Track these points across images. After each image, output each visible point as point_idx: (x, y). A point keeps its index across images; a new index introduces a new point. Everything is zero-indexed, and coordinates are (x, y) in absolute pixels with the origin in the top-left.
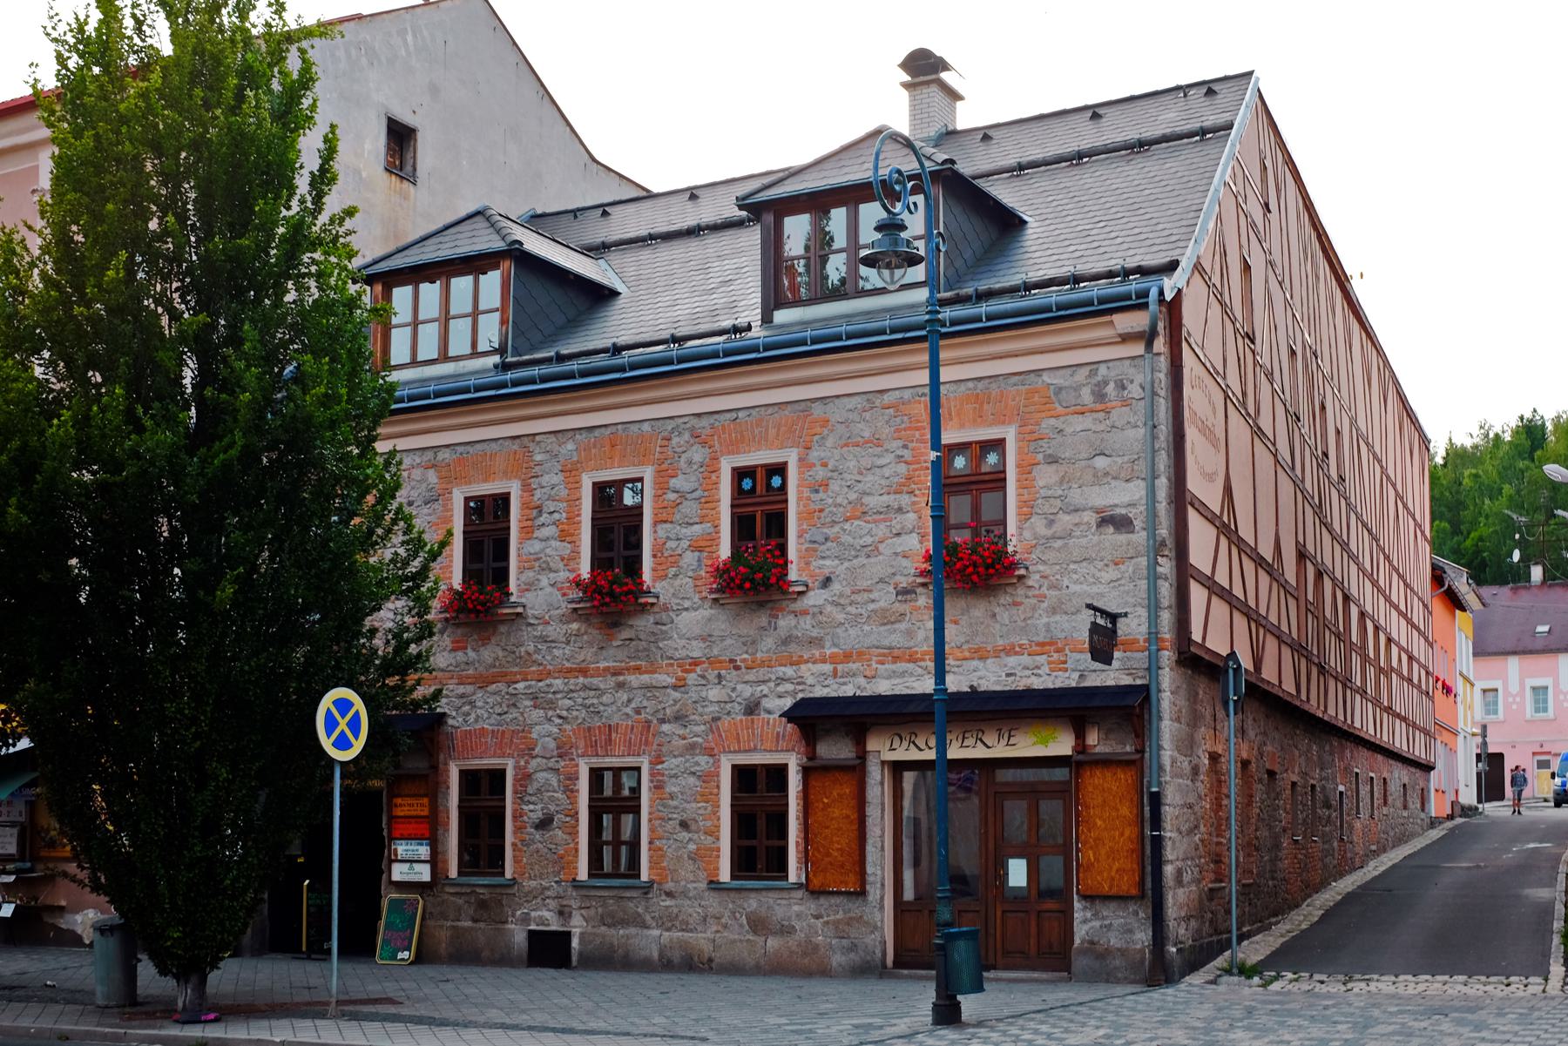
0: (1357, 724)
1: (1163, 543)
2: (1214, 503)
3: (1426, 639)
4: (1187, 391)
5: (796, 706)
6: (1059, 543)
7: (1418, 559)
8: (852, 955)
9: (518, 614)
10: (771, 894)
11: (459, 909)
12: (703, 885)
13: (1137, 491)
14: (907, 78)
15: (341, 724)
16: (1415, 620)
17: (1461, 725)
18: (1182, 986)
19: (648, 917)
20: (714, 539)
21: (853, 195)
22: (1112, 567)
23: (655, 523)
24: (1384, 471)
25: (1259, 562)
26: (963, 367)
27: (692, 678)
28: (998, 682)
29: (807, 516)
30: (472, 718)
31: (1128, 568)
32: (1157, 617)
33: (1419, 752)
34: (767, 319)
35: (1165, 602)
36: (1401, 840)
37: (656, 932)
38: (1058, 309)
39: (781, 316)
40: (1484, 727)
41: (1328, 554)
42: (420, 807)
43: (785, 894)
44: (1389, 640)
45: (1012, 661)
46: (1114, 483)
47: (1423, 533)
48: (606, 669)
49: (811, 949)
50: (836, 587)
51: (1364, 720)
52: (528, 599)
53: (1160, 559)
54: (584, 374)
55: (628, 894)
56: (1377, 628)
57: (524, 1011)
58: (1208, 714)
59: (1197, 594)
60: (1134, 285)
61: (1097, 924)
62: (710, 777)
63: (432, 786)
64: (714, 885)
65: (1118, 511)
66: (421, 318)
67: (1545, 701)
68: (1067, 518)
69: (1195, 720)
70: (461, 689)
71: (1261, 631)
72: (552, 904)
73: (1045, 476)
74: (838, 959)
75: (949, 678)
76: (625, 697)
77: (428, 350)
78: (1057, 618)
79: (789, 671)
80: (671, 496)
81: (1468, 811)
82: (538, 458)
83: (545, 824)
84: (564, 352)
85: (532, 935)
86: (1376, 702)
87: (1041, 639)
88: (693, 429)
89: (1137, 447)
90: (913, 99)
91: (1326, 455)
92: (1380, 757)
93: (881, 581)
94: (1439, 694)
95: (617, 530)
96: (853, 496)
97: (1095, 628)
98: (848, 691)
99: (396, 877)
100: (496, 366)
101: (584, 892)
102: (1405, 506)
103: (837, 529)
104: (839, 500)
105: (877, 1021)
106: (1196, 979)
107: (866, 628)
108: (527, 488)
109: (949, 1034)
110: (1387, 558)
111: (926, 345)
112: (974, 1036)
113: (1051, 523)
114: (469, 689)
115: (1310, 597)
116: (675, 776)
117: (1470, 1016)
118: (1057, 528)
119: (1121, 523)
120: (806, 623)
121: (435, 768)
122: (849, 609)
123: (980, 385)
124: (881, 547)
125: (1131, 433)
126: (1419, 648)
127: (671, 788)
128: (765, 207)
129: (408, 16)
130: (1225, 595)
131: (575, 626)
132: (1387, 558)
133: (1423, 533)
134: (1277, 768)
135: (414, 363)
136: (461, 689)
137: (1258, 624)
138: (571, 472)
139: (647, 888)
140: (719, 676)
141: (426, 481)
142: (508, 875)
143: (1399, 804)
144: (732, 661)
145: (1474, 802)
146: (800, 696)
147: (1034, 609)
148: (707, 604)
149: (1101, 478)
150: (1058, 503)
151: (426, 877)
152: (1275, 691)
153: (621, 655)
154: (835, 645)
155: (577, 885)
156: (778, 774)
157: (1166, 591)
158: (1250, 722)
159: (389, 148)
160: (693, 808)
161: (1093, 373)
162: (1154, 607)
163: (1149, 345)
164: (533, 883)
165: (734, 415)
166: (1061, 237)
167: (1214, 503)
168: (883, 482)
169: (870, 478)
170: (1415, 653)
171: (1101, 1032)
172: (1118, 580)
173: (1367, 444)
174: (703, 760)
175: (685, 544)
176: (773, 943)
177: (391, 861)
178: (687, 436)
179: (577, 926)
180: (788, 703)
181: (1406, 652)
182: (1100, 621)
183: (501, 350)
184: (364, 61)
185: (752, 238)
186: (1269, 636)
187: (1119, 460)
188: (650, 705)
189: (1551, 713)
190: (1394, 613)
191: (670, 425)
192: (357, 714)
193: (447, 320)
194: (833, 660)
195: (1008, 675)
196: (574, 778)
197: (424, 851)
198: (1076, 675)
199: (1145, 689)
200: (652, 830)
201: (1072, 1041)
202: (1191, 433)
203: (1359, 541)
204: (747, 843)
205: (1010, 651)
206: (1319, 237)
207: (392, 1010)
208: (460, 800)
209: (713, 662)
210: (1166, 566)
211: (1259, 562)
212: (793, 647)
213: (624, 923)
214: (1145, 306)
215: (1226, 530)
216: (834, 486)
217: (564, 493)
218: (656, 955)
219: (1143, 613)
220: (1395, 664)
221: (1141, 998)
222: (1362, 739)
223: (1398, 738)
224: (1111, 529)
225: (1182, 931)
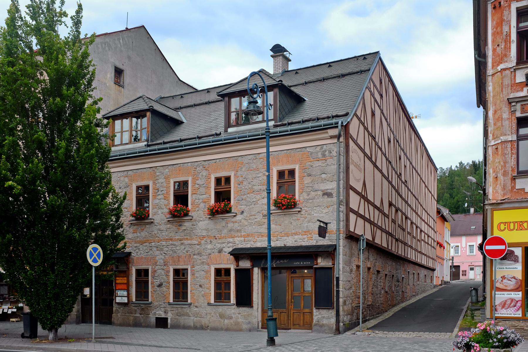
1: (342, 201)
2: (359, 189)
3: (434, 231)
4: (351, 153)
5: (233, 250)
6: (311, 201)
7: (432, 206)
8: (249, 325)
9: (152, 222)
10: (226, 307)
11: (136, 311)
12: (206, 304)
13: (334, 185)
14: (272, 53)
15: (94, 254)
16: (430, 225)
17: (445, 257)
18: (344, 335)
19: (190, 313)
20: (209, 199)
21: (241, 94)
22: (326, 208)
23: (192, 194)
24: (421, 179)
25: (375, 207)
26: (277, 147)
27: (203, 242)
28: (292, 243)
29: (236, 192)
30: (139, 253)
31: (331, 208)
32: (339, 224)
33: (430, 265)
34: (226, 131)
35: (342, 219)
36: (424, 291)
37: (192, 318)
38: (311, 128)
39: (230, 130)
40: (453, 257)
41: (400, 204)
42: (124, 280)
43: (229, 307)
44: (421, 231)
45: (296, 237)
46: (327, 182)
47: (434, 198)
48: (178, 239)
49: (237, 323)
50: (245, 214)
51: (411, 255)
52: (155, 217)
53: (341, 206)
54: (170, 148)
55: (184, 306)
56: (417, 227)
57: (149, 341)
58: (356, 254)
59: (353, 217)
60: (334, 121)
61: (320, 316)
62: (208, 272)
63: (126, 273)
64: (209, 304)
66: (124, 130)
67: (473, 250)
68: (313, 193)
69: (351, 255)
70: (136, 245)
71: (375, 228)
72: (163, 309)
74: (245, 326)
75: (272, 243)
76: (183, 247)
78: (310, 224)
79: (231, 240)
80: (197, 186)
81: (446, 283)
82: (158, 174)
83: (160, 285)
84: (165, 141)
85: (157, 318)
86: (416, 250)
87: (305, 230)
88: (203, 165)
89: (335, 171)
90: (275, 61)
91: (401, 174)
92: (417, 267)
93: (258, 212)
94: (438, 248)
95: (181, 198)
96: (250, 186)
97: (320, 227)
98: (248, 246)
99: (117, 301)
100: (145, 146)
101: (172, 306)
102: (428, 189)
103: (245, 196)
104: (246, 187)
105: (251, 344)
106: (348, 333)
107: (254, 227)
108: (154, 183)
109: (270, 348)
110: (421, 205)
111: (265, 140)
112: (277, 349)
113: (308, 195)
114: (138, 245)
116: (198, 271)
117: (425, 344)
118: (310, 196)
119: (328, 194)
120: (236, 225)
121: (128, 268)
122: (249, 221)
123: (288, 152)
124: (258, 202)
125: (333, 167)
126: (431, 233)
127: (197, 275)
128: (226, 94)
129: (121, 34)
130: (363, 217)
131: (169, 226)
132: (421, 205)
133: (434, 198)
134: (380, 270)
135: (122, 144)
136: (136, 245)
137: (374, 226)
138: (167, 178)
139: (190, 304)
140: (211, 241)
141: (123, 180)
142: (150, 301)
143: (423, 281)
144: (214, 237)
145: (449, 280)
146: (234, 247)
147: (303, 221)
148: (207, 219)
149: (324, 181)
150: (311, 188)
151: (126, 301)
152: (380, 246)
153: (183, 234)
154: (245, 232)
155: (170, 304)
156: (463, 275)
157: (342, 216)
158: (371, 256)
159: (115, 76)
160: (203, 281)
161: (322, 148)
162: (339, 221)
163: (339, 139)
164: (157, 303)
165: (215, 161)
166: (316, 104)
168: (259, 182)
169: (255, 180)
170: (430, 235)
171: (315, 348)
172: (328, 212)
173: (415, 170)
174: (206, 267)
175: (201, 201)
176: (226, 321)
177: (116, 296)
178: (201, 167)
179: (170, 316)
180: (231, 249)
181: (427, 234)
182: (322, 225)
183: (147, 141)
184: (107, 48)
185: (222, 105)
186: (378, 230)
188: (191, 250)
189: (459, 254)
190: (423, 223)
191: (196, 164)
192: (99, 252)
194: (244, 236)
195: (295, 241)
196: (168, 272)
197: (125, 293)
198: (315, 241)
199: (335, 245)
200: (191, 288)
201: (305, 351)
202: (352, 167)
203: (412, 201)
204: (219, 291)
205: (296, 234)
206: (400, 105)
207: (111, 340)
208: (136, 278)
209: (209, 236)
210: (343, 208)
211: (375, 207)
212: (232, 233)
213: (183, 315)
214: (337, 127)
216: (245, 183)
218: (192, 325)
219: (335, 222)
223: (424, 261)
224: (326, 197)
225: (345, 319)
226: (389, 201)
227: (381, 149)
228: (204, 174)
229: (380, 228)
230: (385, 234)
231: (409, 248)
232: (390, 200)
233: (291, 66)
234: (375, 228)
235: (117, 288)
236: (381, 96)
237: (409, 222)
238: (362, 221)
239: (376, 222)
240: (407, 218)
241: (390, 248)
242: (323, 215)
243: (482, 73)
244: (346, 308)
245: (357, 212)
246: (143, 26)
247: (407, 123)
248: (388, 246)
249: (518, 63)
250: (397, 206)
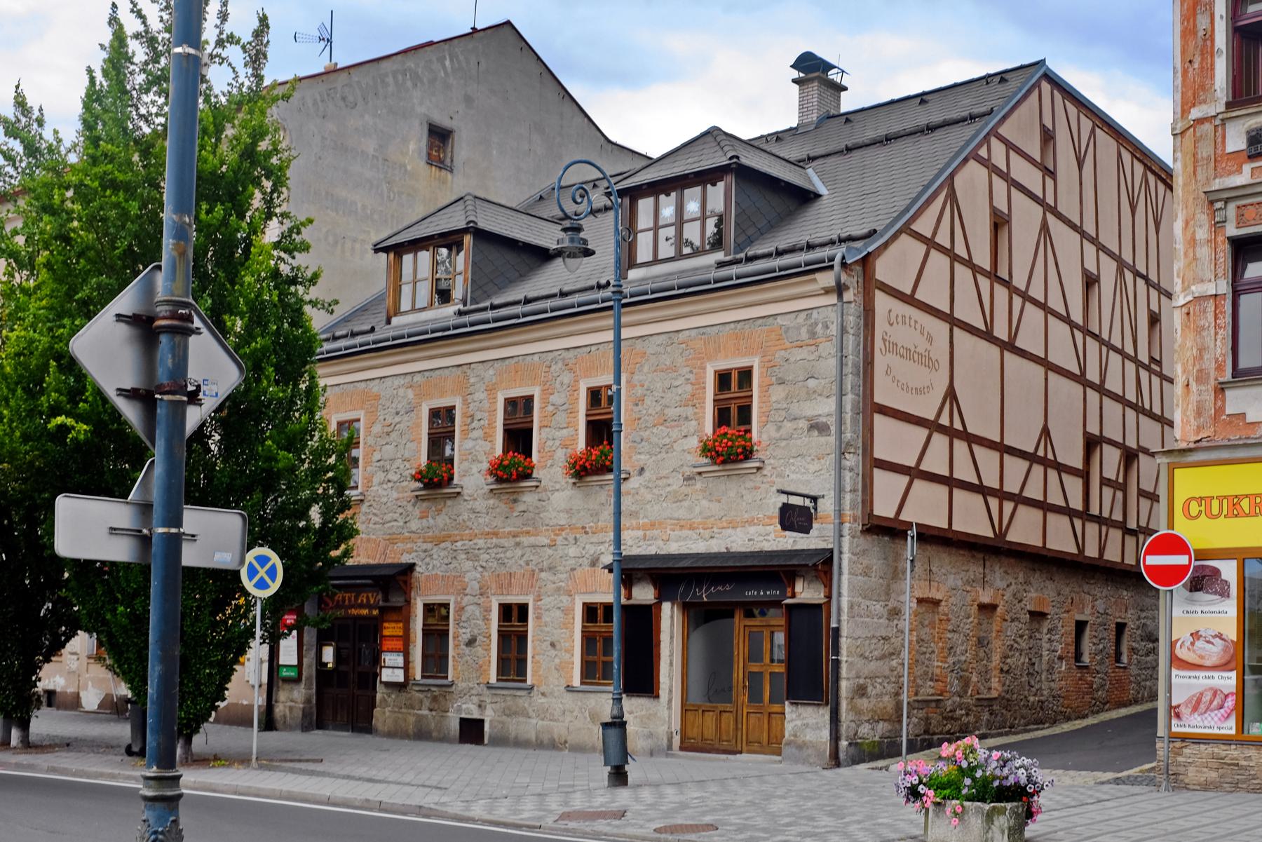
13: (829, 406)
82: (472, 380)
119: (818, 427)
138: (491, 390)
151: (401, 679)
161: (809, 317)
175: (557, 443)
187: (823, 382)
216: (648, 401)
233: (848, 103)
246: (508, 23)
249: (1229, 106)
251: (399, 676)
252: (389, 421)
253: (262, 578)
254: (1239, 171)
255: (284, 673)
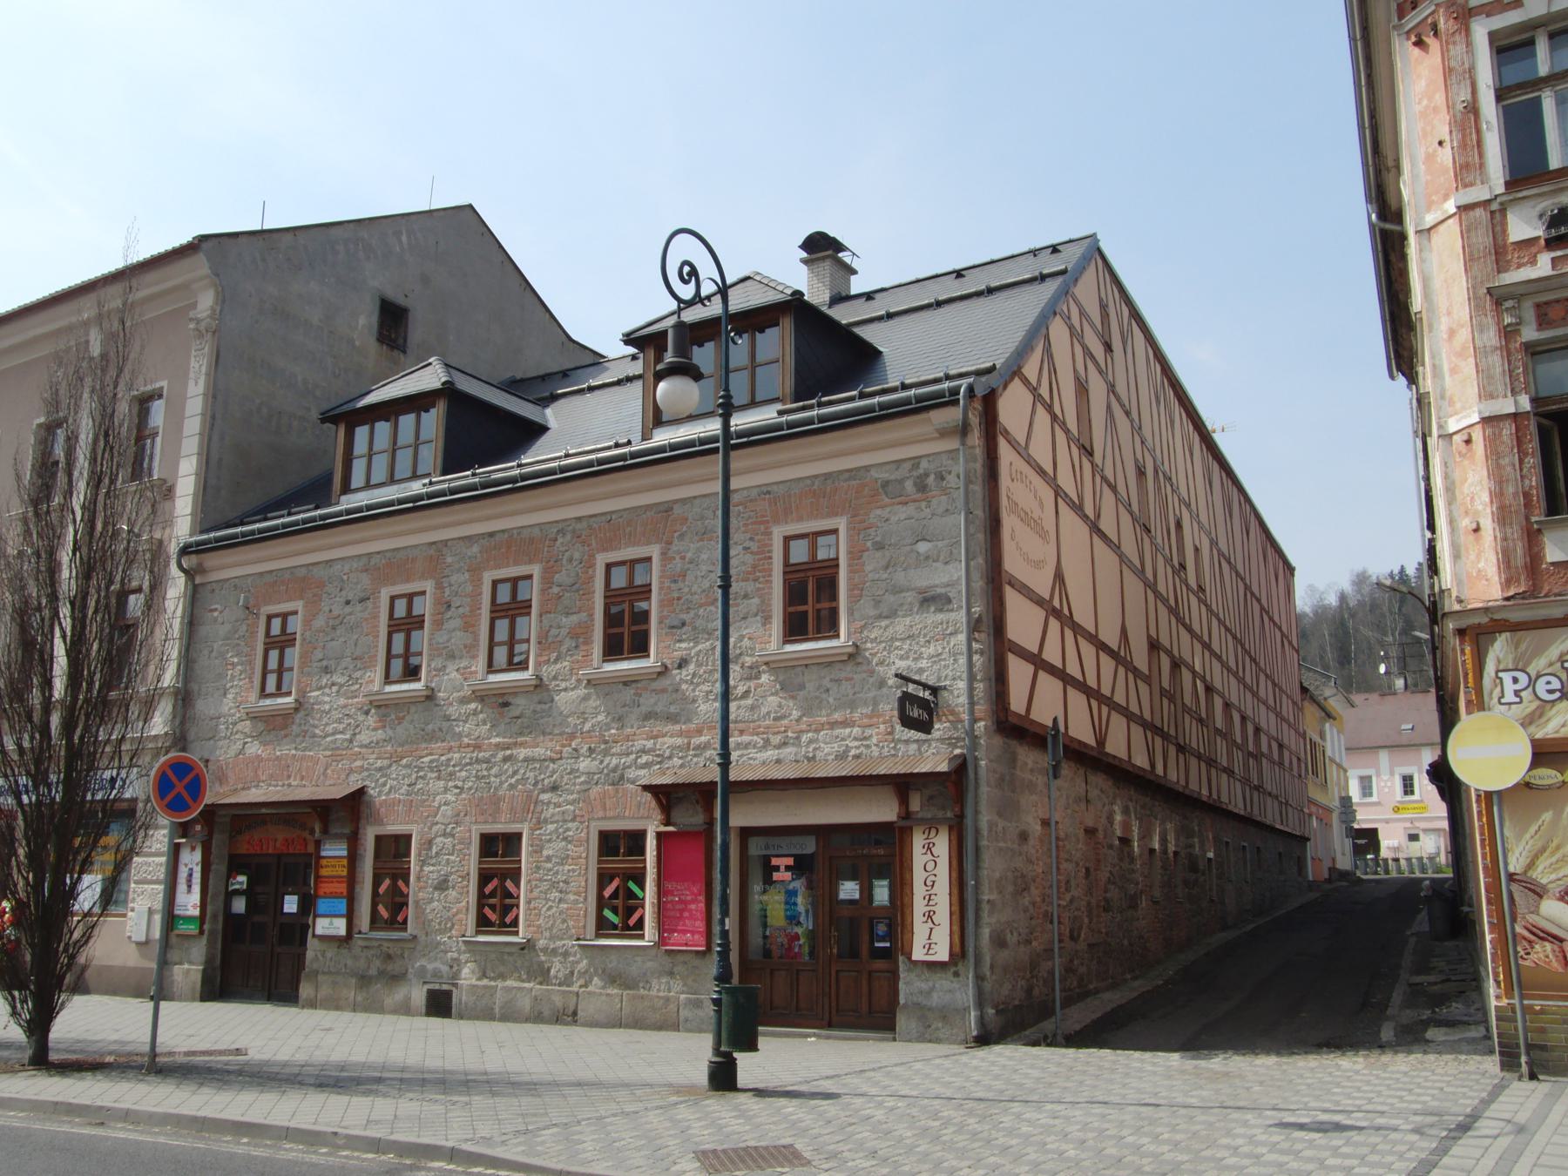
0: (1225, 799)
2: (1042, 583)
13: (958, 571)
14: (804, 255)
24: (1247, 588)
25: (1102, 647)
56: (1244, 719)
65: (939, 590)
71: (1213, 771)
73: (872, 562)
77: (379, 474)
82: (449, 560)
91: (1183, 566)
99: (319, 931)
102: (1271, 619)
108: (439, 587)
110: (1253, 660)
115: (1166, 684)
116: (549, 841)
119: (932, 600)
131: (473, 706)
132: (1253, 660)
138: (475, 571)
151: (343, 932)
156: (635, 841)
161: (916, 466)
167: (1042, 583)
172: (941, 654)
175: (564, 632)
177: (316, 916)
181: (1277, 740)
187: (940, 544)
193: (394, 451)
202: (1009, 522)
206: (1170, 380)
214: (955, 403)
215: (1057, 612)
216: (690, 577)
217: (469, 588)
220: (1265, 749)
221: (964, 1059)
222: (1230, 812)
226: (1149, 636)
227: (1113, 488)
228: (577, 555)
229: (1125, 711)
230: (1141, 729)
231: (1224, 777)
232: (1153, 633)
233: (857, 286)
234: (1105, 709)
235: (321, 892)
236: (1108, 347)
237: (1218, 702)
238: (1057, 685)
239: (1106, 691)
240: (1209, 689)
241: (1160, 770)
242: (924, 664)
243: (1395, 274)
244: (1004, 955)
245: (1110, 699)
246: (471, 206)
247: (1197, 438)
248: (1153, 765)
249: (1510, 185)
250: (1176, 653)
251: (339, 927)
252: (335, 613)
253: (179, 795)
254: (1533, 262)
255: (184, 928)
